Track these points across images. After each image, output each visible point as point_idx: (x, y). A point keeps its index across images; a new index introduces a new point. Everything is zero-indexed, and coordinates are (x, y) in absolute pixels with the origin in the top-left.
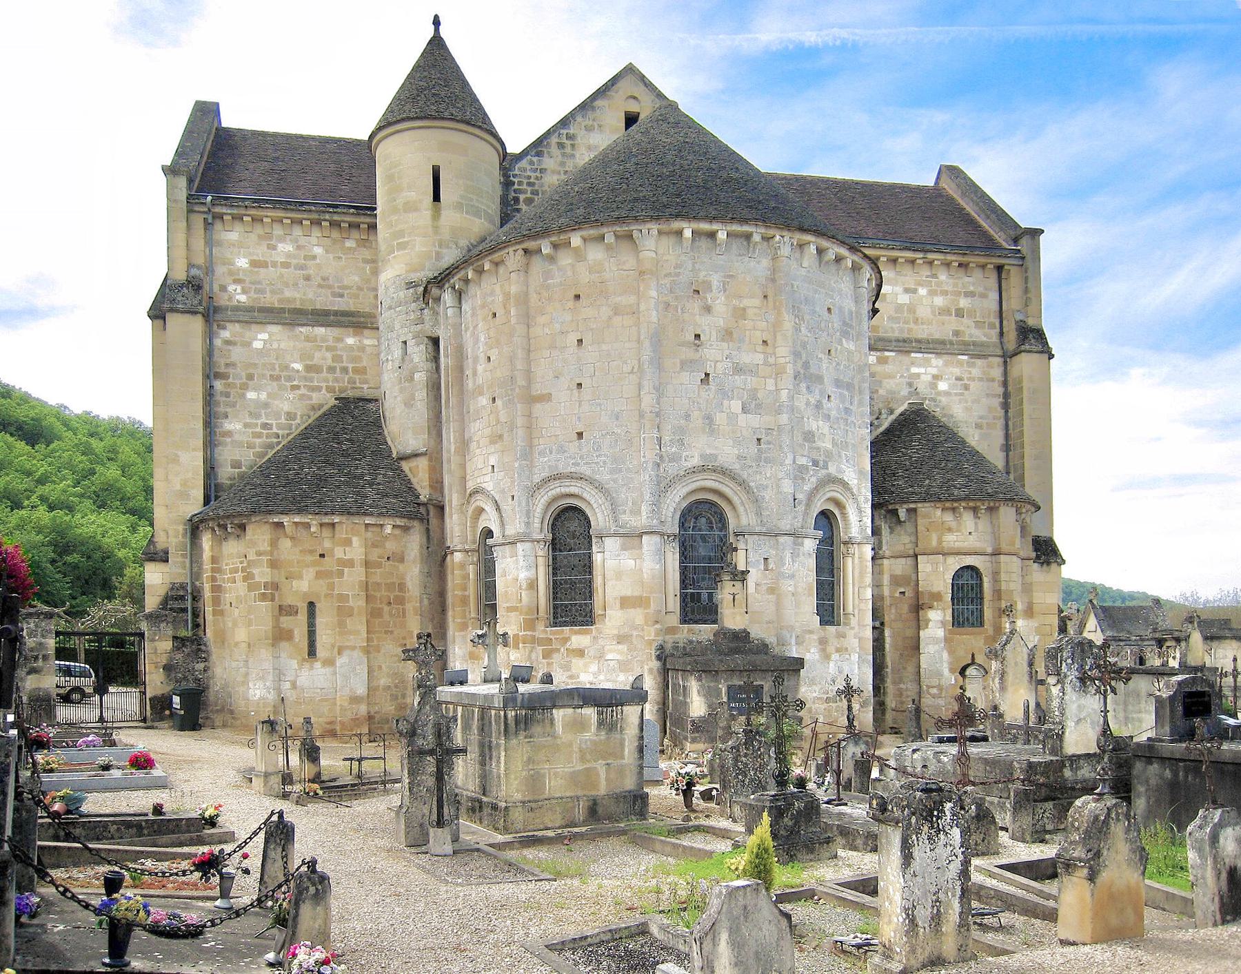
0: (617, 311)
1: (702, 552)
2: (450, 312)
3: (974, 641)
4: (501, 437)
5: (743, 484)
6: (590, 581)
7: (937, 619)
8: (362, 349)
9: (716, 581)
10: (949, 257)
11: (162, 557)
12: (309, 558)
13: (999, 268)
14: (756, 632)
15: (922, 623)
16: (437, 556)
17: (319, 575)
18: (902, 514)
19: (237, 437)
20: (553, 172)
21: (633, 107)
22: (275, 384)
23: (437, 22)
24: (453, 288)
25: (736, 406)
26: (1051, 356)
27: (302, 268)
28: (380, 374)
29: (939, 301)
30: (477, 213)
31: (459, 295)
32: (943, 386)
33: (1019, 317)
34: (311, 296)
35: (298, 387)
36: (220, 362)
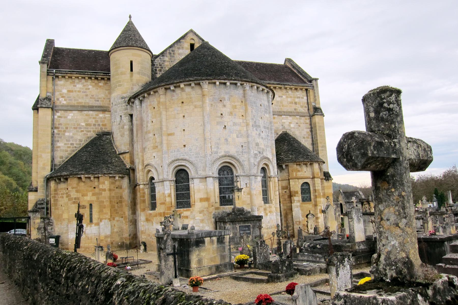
0: (196, 107)
1: (226, 182)
2: (138, 107)
3: (309, 206)
4: (157, 147)
5: (238, 160)
6: (189, 193)
7: (298, 198)
8: (105, 118)
10: (292, 87)
12: (90, 189)
15: (292, 201)
16: (134, 186)
17: (93, 195)
18: (284, 167)
19: (62, 148)
20: (167, 61)
21: (192, 42)
22: (75, 130)
23: (130, 17)
24: (139, 99)
25: (235, 136)
28: (112, 126)
29: (289, 100)
30: (144, 74)
31: (141, 101)
32: (292, 126)
33: (313, 104)
34: (87, 101)
35: (83, 131)
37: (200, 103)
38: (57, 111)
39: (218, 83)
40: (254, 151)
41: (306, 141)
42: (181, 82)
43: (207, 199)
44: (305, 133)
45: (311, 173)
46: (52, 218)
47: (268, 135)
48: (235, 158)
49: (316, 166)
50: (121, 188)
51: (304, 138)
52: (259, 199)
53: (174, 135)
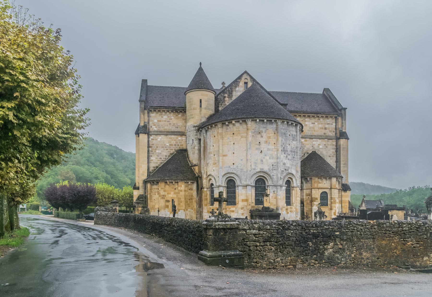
0: (242, 137)
5: (269, 175)
11: (138, 189)
13: (336, 117)
14: (272, 207)
16: (200, 189)
17: (174, 193)
18: (308, 179)
19: (154, 161)
21: (246, 81)
23: (201, 64)
25: (267, 158)
26: (348, 139)
27: (168, 122)
29: (320, 126)
30: (209, 109)
31: (206, 131)
32: (321, 147)
33: (341, 129)
37: (245, 134)
38: (151, 135)
39: (258, 121)
40: (281, 168)
41: (331, 159)
43: (247, 200)
44: (331, 153)
45: (329, 185)
46: (149, 207)
47: (294, 157)
48: (267, 174)
49: (334, 180)
50: (192, 190)
51: (330, 156)
52: (282, 203)
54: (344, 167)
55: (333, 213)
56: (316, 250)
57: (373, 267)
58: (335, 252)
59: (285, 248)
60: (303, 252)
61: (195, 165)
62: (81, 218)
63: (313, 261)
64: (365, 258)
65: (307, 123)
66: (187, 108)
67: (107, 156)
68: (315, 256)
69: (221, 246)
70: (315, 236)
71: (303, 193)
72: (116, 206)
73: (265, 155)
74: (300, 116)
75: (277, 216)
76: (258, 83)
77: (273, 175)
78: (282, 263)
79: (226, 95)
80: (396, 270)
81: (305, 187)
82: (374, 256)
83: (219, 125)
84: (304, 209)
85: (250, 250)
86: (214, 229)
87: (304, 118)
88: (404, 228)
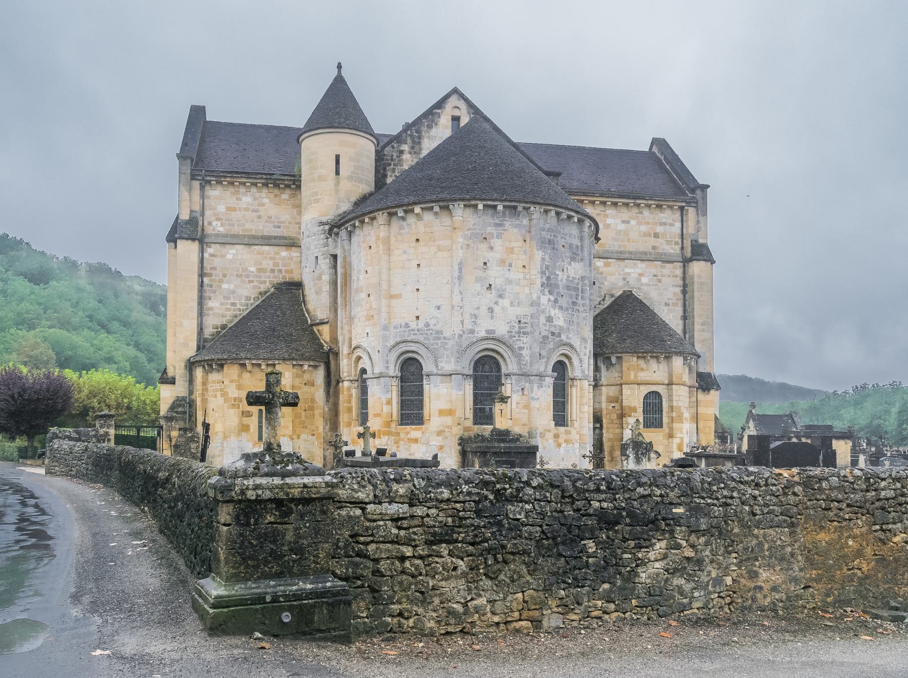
0: (439, 249)
4: (372, 316)
5: (510, 347)
8: (291, 258)
9: (493, 401)
11: (172, 382)
13: (682, 209)
14: (517, 430)
16: (332, 382)
18: (614, 360)
19: (216, 311)
21: (457, 113)
23: (339, 67)
24: (347, 229)
26: (713, 262)
29: (644, 228)
30: (360, 181)
31: (350, 234)
34: (261, 227)
35: (252, 282)
36: (207, 270)
38: (209, 244)
39: (480, 207)
42: (415, 203)
43: (450, 412)
45: (666, 375)
47: (574, 303)
48: (504, 344)
49: (677, 362)
50: (313, 385)
51: (667, 304)
52: (544, 418)
53: (400, 298)
54: (703, 331)
55: (675, 446)
56: (609, 567)
57: (795, 618)
58: (672, 572)
59: (505, 562)
60: (565, 573)
61: (322, 323)
62: (32, 457)
63: (599, 603)
64: (766, 587)
65: (609, 221)
66: (303, 179)
67: (140, 307)
68: (606, 586)
69: (266, 563)
70: (607, 521)
71: (600, 395)
72: (109, 426)
73: (501, 296)
74: (593, 203)
75: (530, 452)
76: (487, 119)
77: (521, 348)
78: (494, 613)
79: (405, 147)
80: (864, 625)
81: (604, 381)
82: (795, 580)
83: (382, 217)
84: (601, 434)
85: (377, 572)
86: (240, 502)
87: (602, 208)
88: (883, 493)
